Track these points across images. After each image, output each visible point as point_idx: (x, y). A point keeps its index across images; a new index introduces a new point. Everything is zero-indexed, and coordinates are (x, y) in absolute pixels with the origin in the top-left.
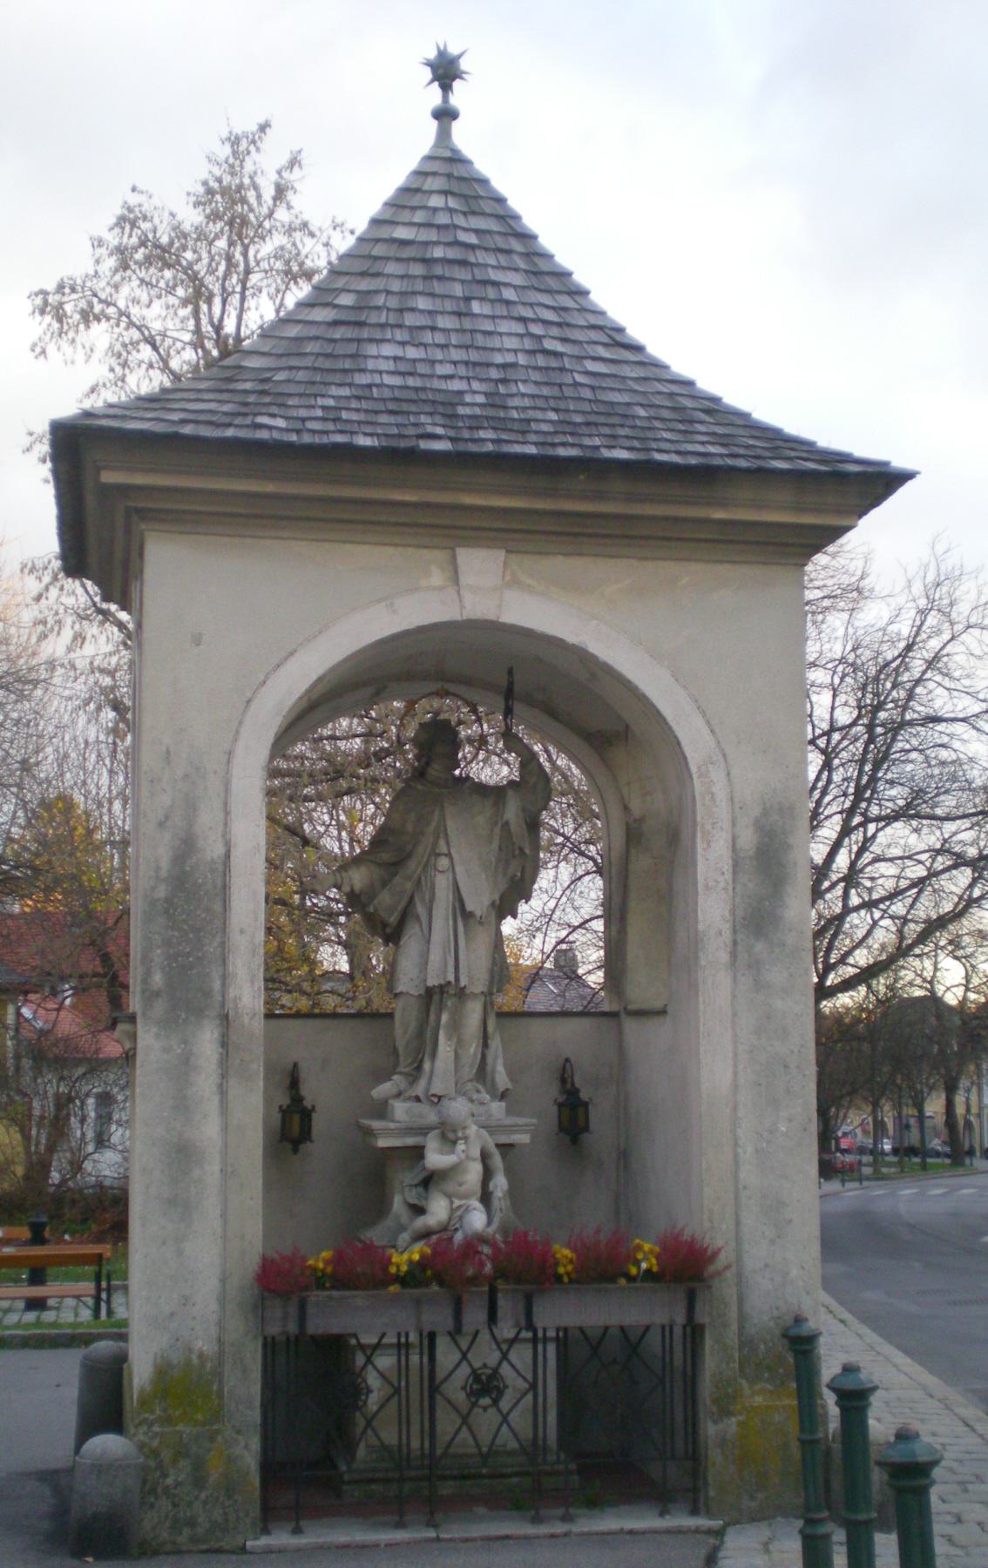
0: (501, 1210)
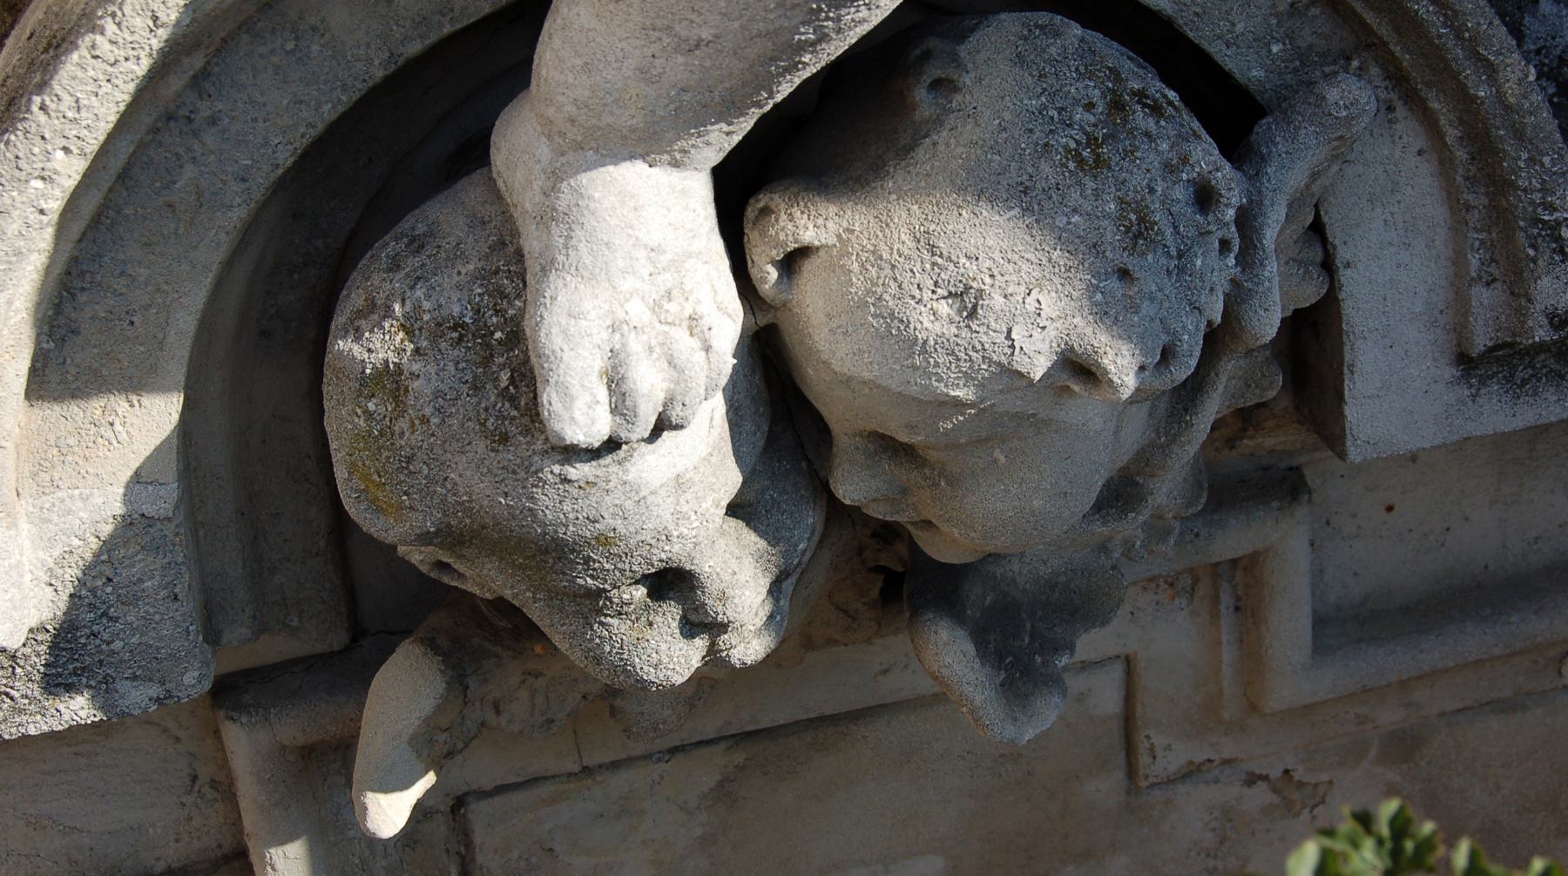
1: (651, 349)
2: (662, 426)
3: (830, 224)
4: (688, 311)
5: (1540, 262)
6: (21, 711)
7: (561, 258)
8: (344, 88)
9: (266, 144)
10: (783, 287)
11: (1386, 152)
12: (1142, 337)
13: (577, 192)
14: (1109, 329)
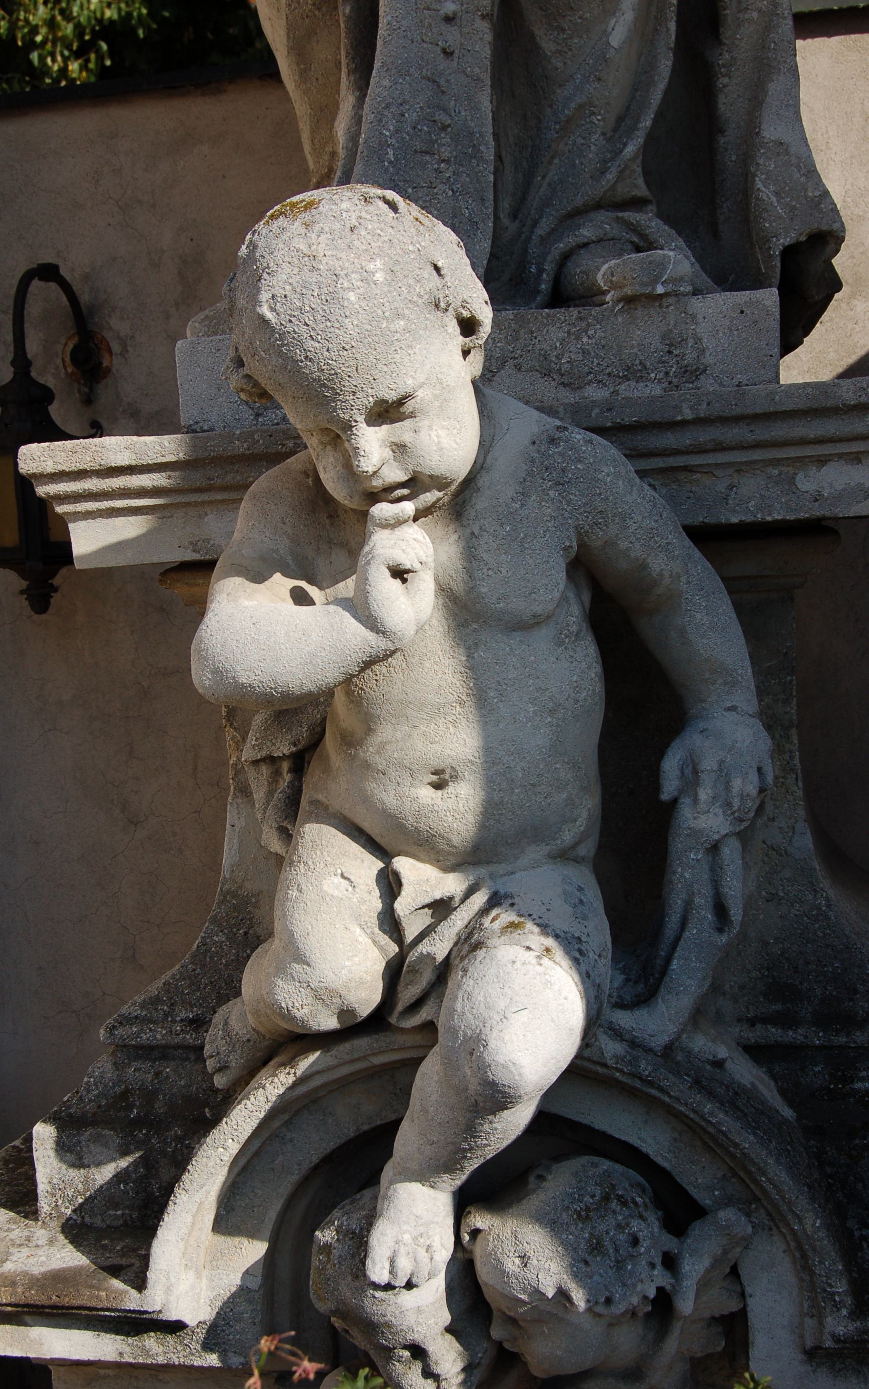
0: (721, 910)
1: (408, 1253)
2: (410, 1285)
3: (487, 1222)
4: (428, 1243)
5: (827, 1310)
6: (193, 1355)
7: (384, 1213)
8: (339, 1137)
9: (309, 1153)
10: (471, 1243)
11: (769, 1248)
12: (590, 1289)
13: (394, 1190)
14: (577, 1283)
